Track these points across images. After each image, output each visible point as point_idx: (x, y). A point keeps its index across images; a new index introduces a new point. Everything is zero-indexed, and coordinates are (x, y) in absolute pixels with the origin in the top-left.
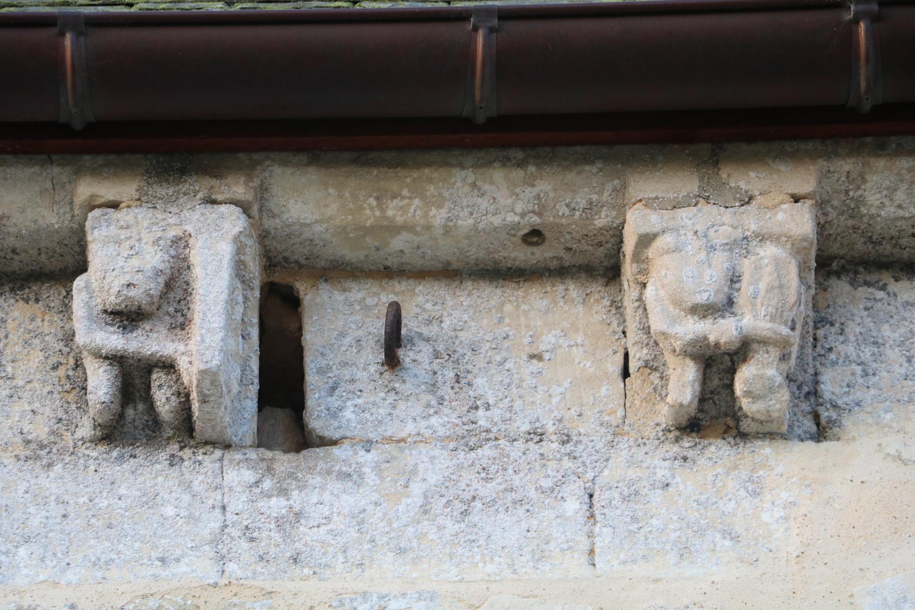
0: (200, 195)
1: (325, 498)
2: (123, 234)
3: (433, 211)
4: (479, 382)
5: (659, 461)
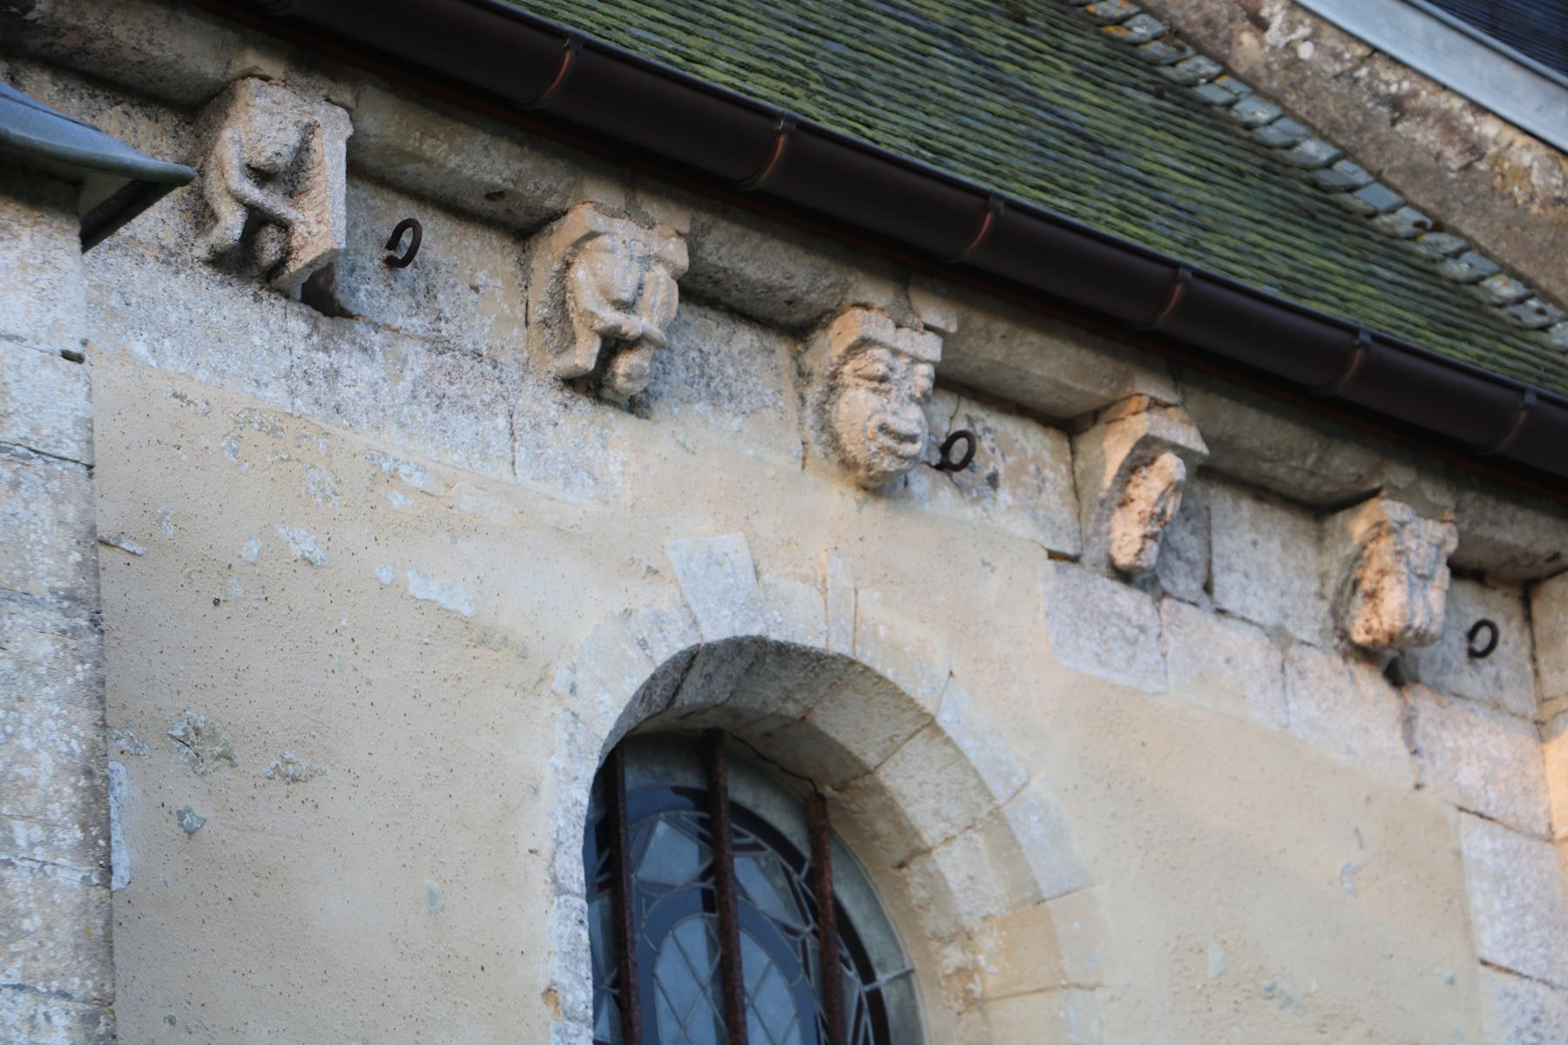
0: (323, 92)
1: (359, 369)
2: (276, 108)
3: (452, 156)
4: (441, 297)
5: (549, 402)
